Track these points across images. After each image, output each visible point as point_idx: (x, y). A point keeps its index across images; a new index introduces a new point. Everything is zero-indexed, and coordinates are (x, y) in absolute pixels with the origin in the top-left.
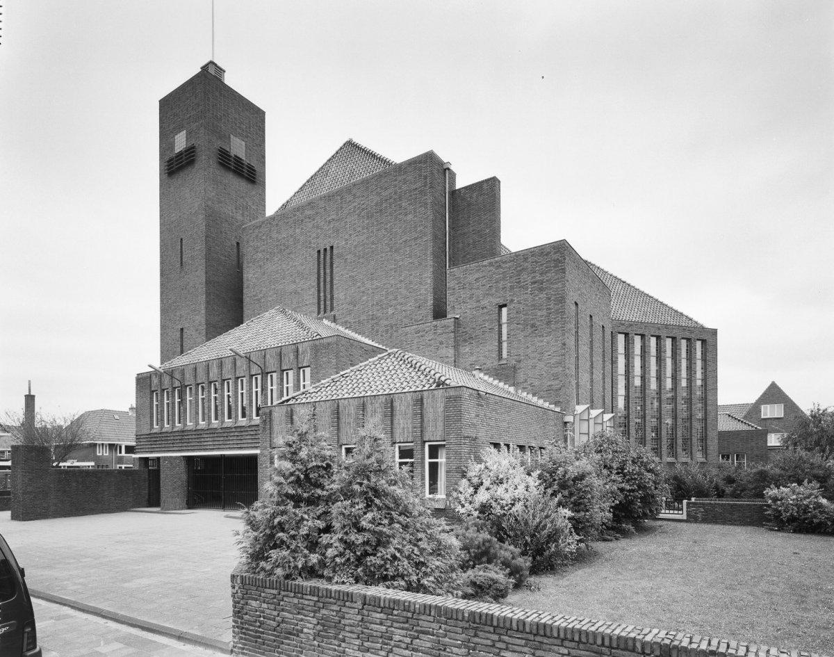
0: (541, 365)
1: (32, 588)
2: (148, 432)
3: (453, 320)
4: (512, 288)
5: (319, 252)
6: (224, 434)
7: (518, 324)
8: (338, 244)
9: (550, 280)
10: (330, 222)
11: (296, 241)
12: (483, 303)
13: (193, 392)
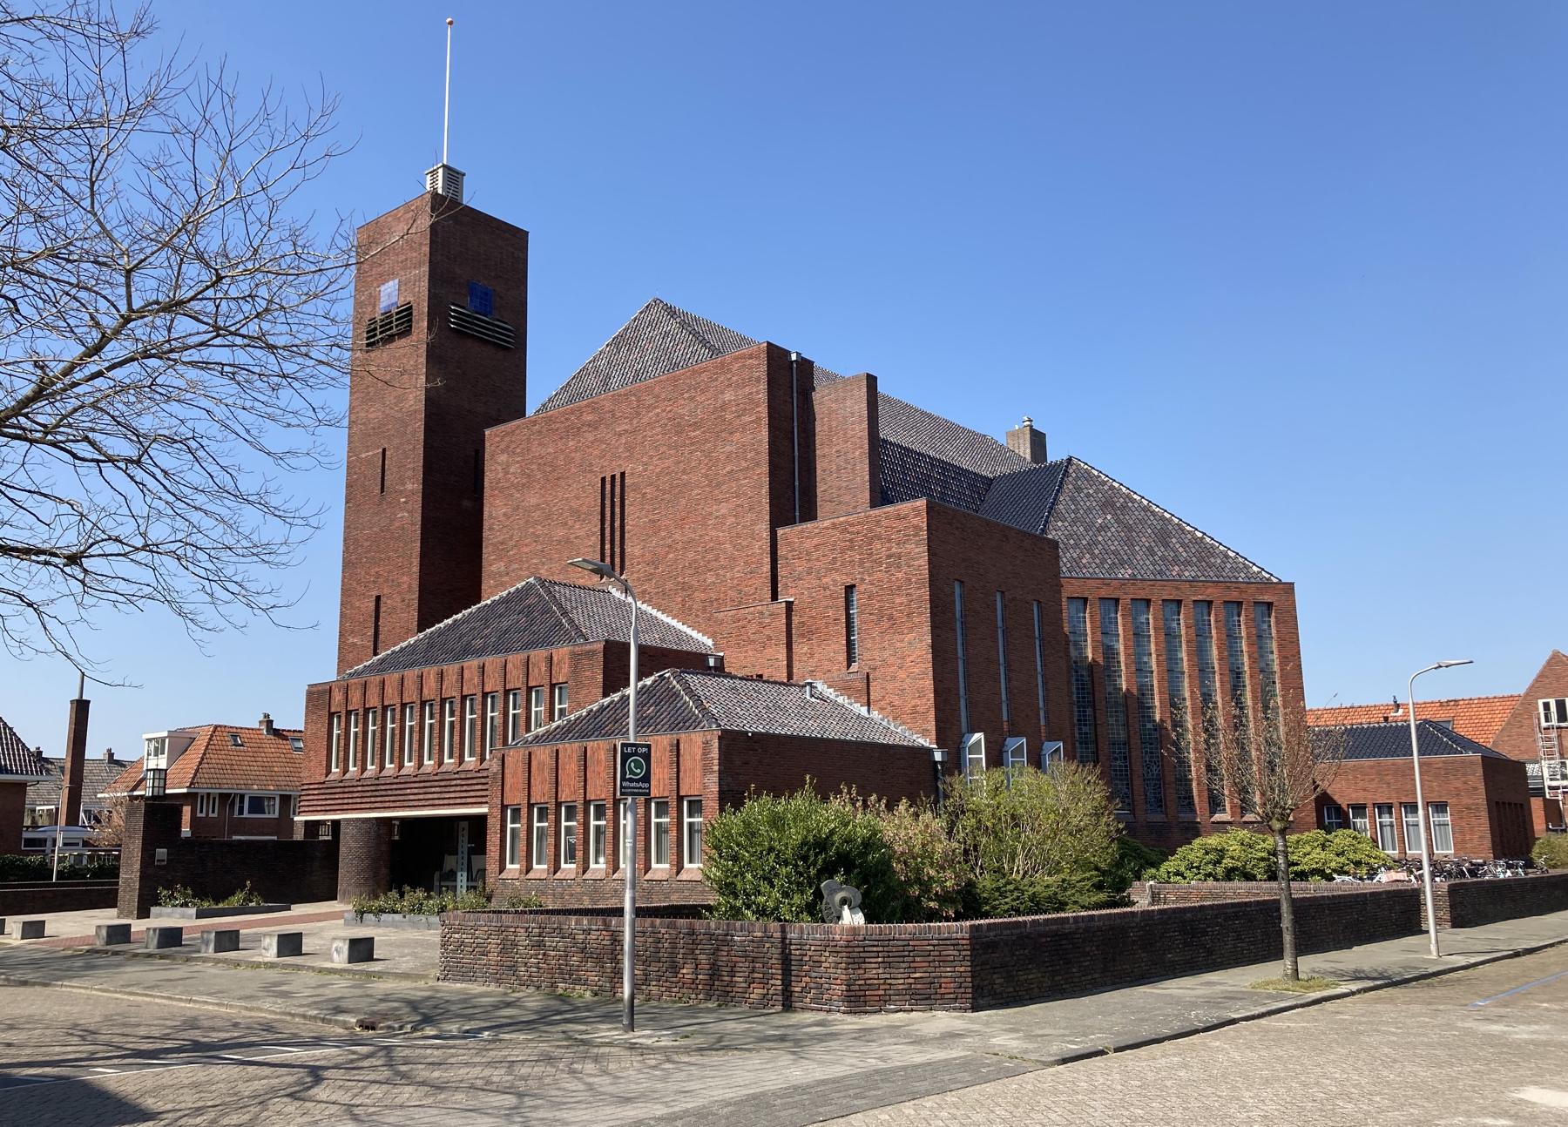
0: (902, 674)
1: (895, 395)
2: (323, 779)
3: (784, 605)
4: (862, 562)
5: (603, 479)
6: (426, 785)
7: (871, 614)
8: (632, 469)
9: (910, 553)
10: (620, 435)
11: (568, 460)
12: (824, 581)
13: (398, 716)
